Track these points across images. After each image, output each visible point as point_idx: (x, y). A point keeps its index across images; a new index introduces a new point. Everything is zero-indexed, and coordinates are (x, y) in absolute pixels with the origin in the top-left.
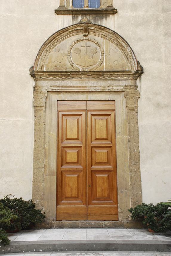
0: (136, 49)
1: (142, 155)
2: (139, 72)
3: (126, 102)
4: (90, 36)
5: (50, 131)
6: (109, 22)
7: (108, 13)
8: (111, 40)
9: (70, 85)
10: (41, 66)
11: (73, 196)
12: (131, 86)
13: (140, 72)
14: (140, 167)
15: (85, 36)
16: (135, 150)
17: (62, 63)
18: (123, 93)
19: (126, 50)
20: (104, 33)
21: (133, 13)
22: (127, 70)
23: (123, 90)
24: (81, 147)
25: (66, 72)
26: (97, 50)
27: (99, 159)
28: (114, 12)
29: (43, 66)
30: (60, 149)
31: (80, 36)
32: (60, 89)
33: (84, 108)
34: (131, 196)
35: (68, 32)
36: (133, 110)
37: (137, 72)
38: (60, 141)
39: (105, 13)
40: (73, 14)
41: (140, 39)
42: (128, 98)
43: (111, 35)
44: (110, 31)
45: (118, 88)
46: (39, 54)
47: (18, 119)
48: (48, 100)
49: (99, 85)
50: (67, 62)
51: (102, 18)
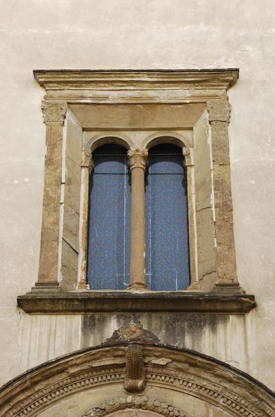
4: (154, 393)
7: (219, 307)
15: (132, 390)
20: (208, 380)
35: (64, 375)
39: (208, 306)
40: (86, 311)
43: (237, 390)
51: (196, 328)
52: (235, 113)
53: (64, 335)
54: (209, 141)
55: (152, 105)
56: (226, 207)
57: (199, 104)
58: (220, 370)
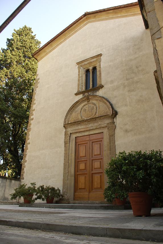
2: (115, 114)
5: (71, 153)
6: (100, 93)
7: (99, 88)
9: (80, 128)
10: (68, 121)
11: (83, 188)
12: (110, 123)
17: (78, 118)
20: (97, 98)
24: (87, 160)
25: (78, 122)
26: (94, 107)
27: (96, 167)
29: (69, 121)
30: (77, 163)
31: (86, 103)
32: (76, 131)
33: (88, 139)
36: (112, 136)
38: (77, 158)
41: (116, 97)
43: (100, 98)
45: (104, 125)
46: (66, 116)
47: (58, 149)
48: (71, 138)
49: (94, 125)
50: (80, 117)
51: (96, 92)
53: (81, 96)
55: (91, 62)
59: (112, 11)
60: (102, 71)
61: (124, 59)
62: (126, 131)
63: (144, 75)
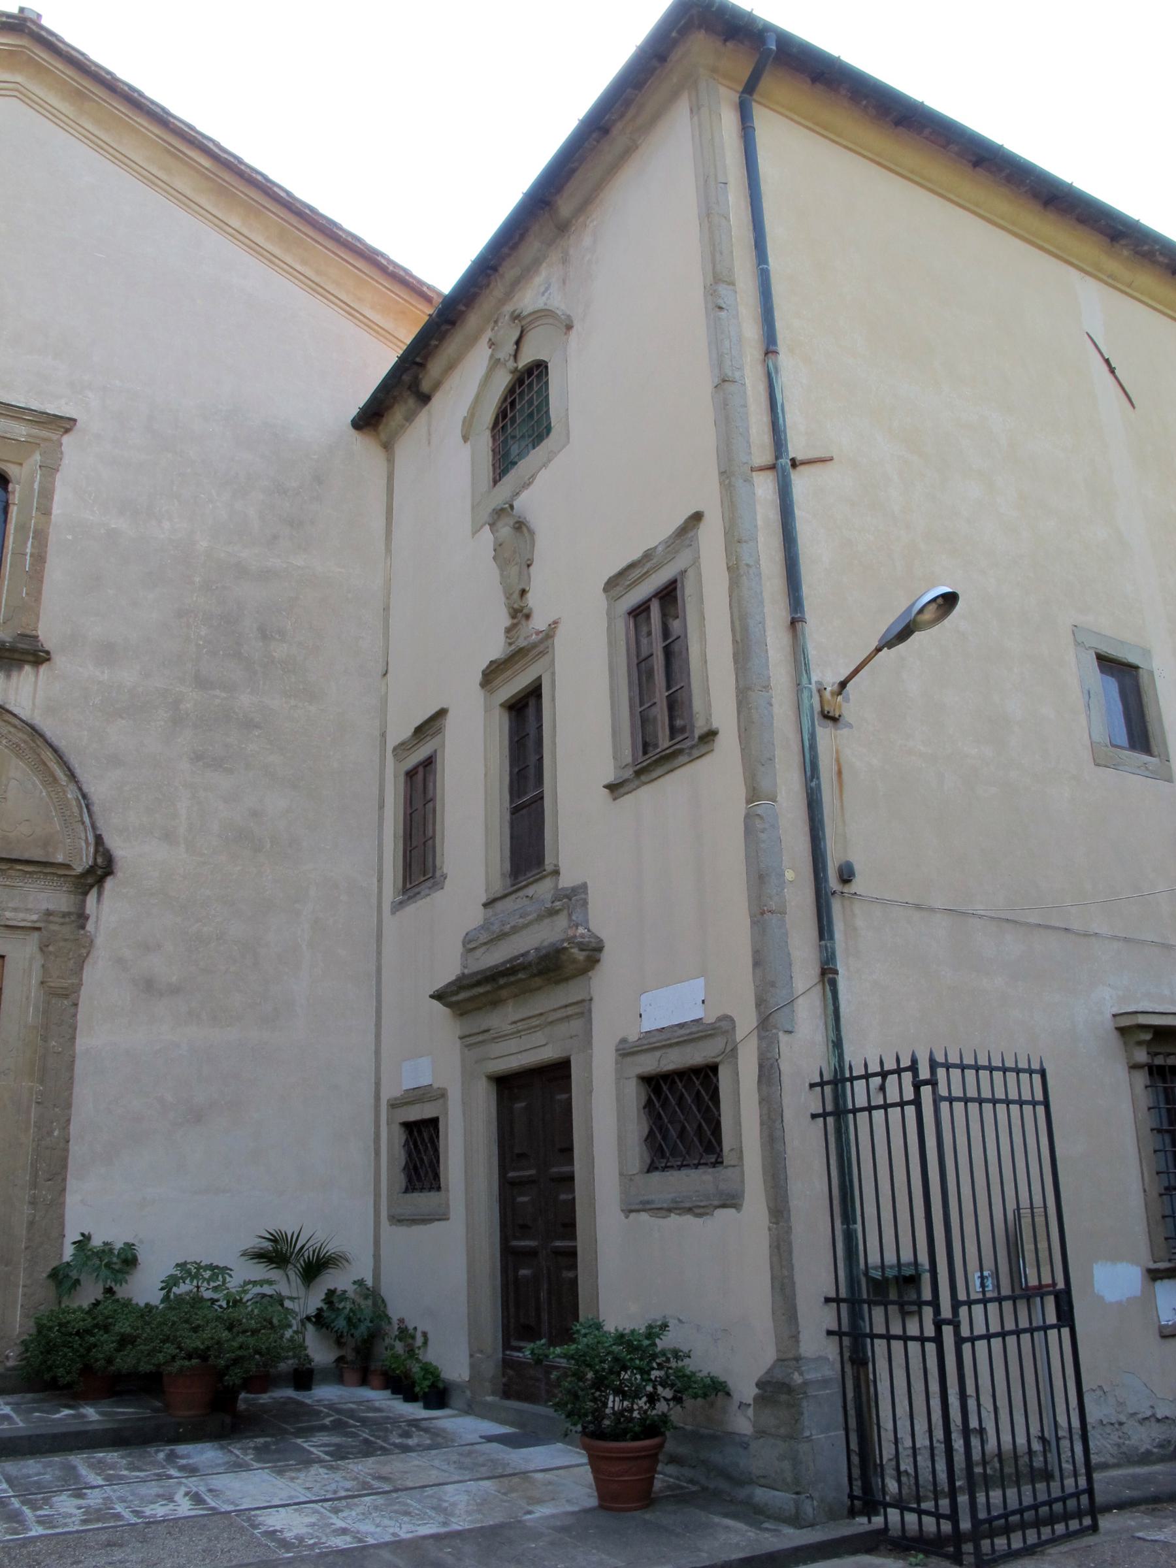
0: (98, 790)
1: (77, 1151)
2: (101, 870)
3: (43, 966)
7: (16, 656)
8: (16, 749)
12: (65, 915)
13: (99, 872)
14: (64, 1190)
16: (56, 1133)
18: (36, 934)
19: (64, 792)
21: (103, 673)
22: (60, 858)
23: (37, 925)
28: (37, 656)
34: (24, 1286)
37: (91, 871)
39: (7, 654)
42: (51, 953)
43: (20, 735)
44: (17, 722)
45: (21, 915)
52: (66, 461)
54: (36, 486)
56: (40, 558)
57: (31, 445)
58: (8, 717)
59: (206, 162)
60: (52, 538)
61: (204, 544)
62: (149, 986)
63: (293, 702)
